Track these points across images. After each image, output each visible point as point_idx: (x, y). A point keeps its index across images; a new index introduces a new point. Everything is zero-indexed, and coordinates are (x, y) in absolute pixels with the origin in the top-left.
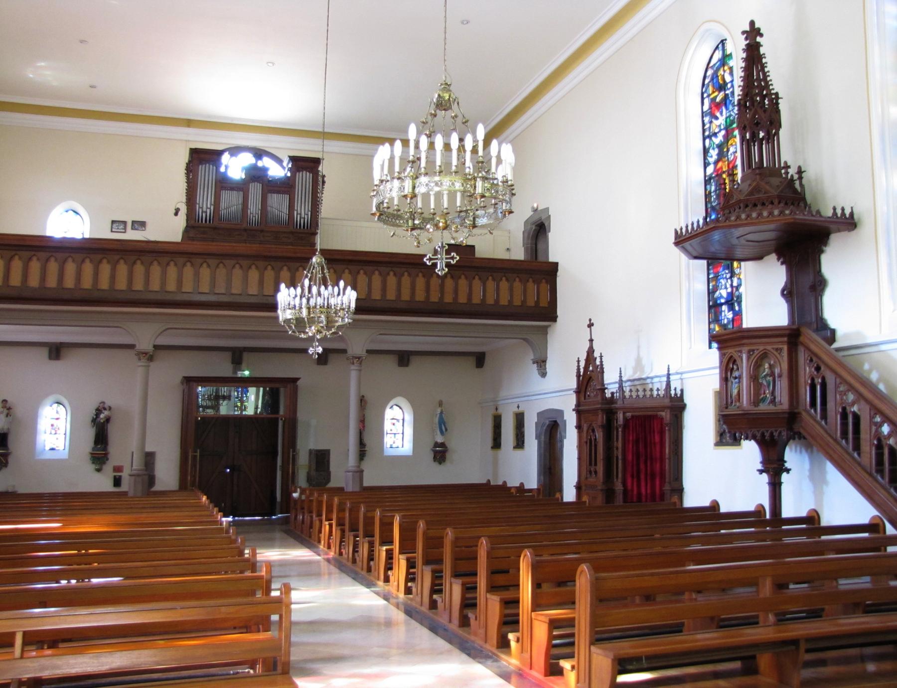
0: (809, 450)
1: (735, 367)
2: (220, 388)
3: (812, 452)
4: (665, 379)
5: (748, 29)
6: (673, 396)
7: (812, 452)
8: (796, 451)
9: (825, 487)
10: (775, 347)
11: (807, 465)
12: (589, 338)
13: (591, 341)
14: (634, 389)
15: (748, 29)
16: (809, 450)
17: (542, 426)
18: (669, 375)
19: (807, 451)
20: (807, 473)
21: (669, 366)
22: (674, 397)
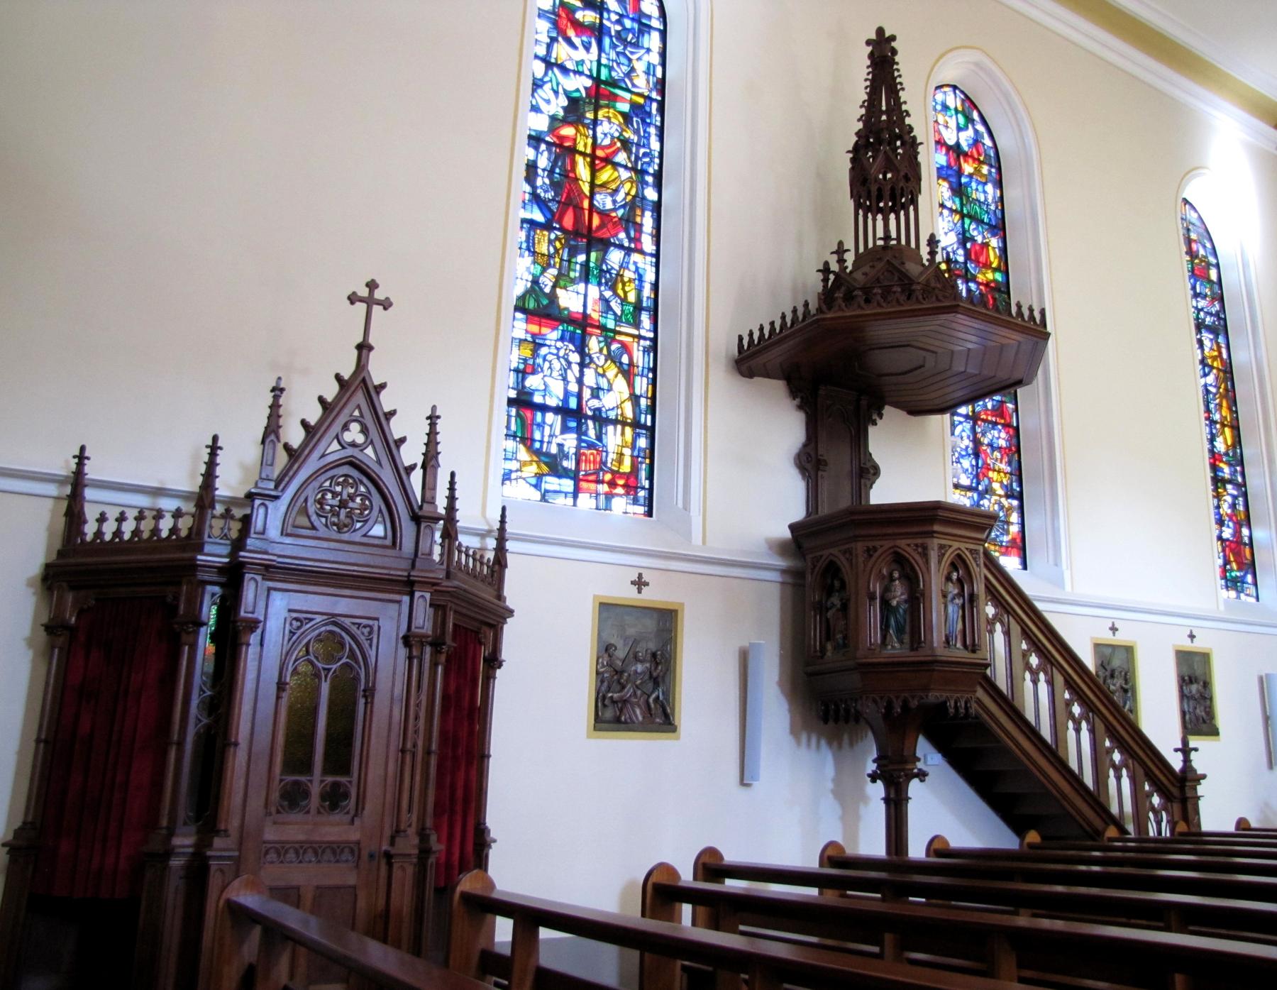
0: (835, 744)
1: (837, 584)
2: (1166, 832)
3: (840, 746)
4: (491, 543)
5: (873, 36)
6: (89, 538)
7: (840, 746)
8: (809, 745)
9: (862, 807)
10: (823, 559)
11: (830, 770)
12: (360, 339)
13: (364, 348)
14: (113, 513)
15: (873, 36)
16: (835, 744)
17: (306, 688)
18: (502, 538)
19: (830, 744)
20: (830, 785)
21: (504, 509)
22: (94, 540)
